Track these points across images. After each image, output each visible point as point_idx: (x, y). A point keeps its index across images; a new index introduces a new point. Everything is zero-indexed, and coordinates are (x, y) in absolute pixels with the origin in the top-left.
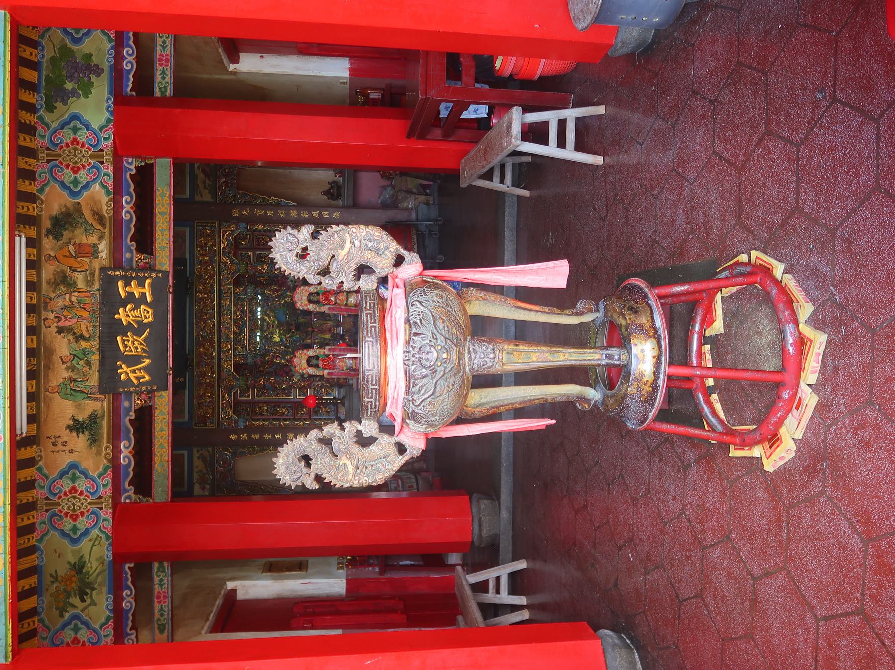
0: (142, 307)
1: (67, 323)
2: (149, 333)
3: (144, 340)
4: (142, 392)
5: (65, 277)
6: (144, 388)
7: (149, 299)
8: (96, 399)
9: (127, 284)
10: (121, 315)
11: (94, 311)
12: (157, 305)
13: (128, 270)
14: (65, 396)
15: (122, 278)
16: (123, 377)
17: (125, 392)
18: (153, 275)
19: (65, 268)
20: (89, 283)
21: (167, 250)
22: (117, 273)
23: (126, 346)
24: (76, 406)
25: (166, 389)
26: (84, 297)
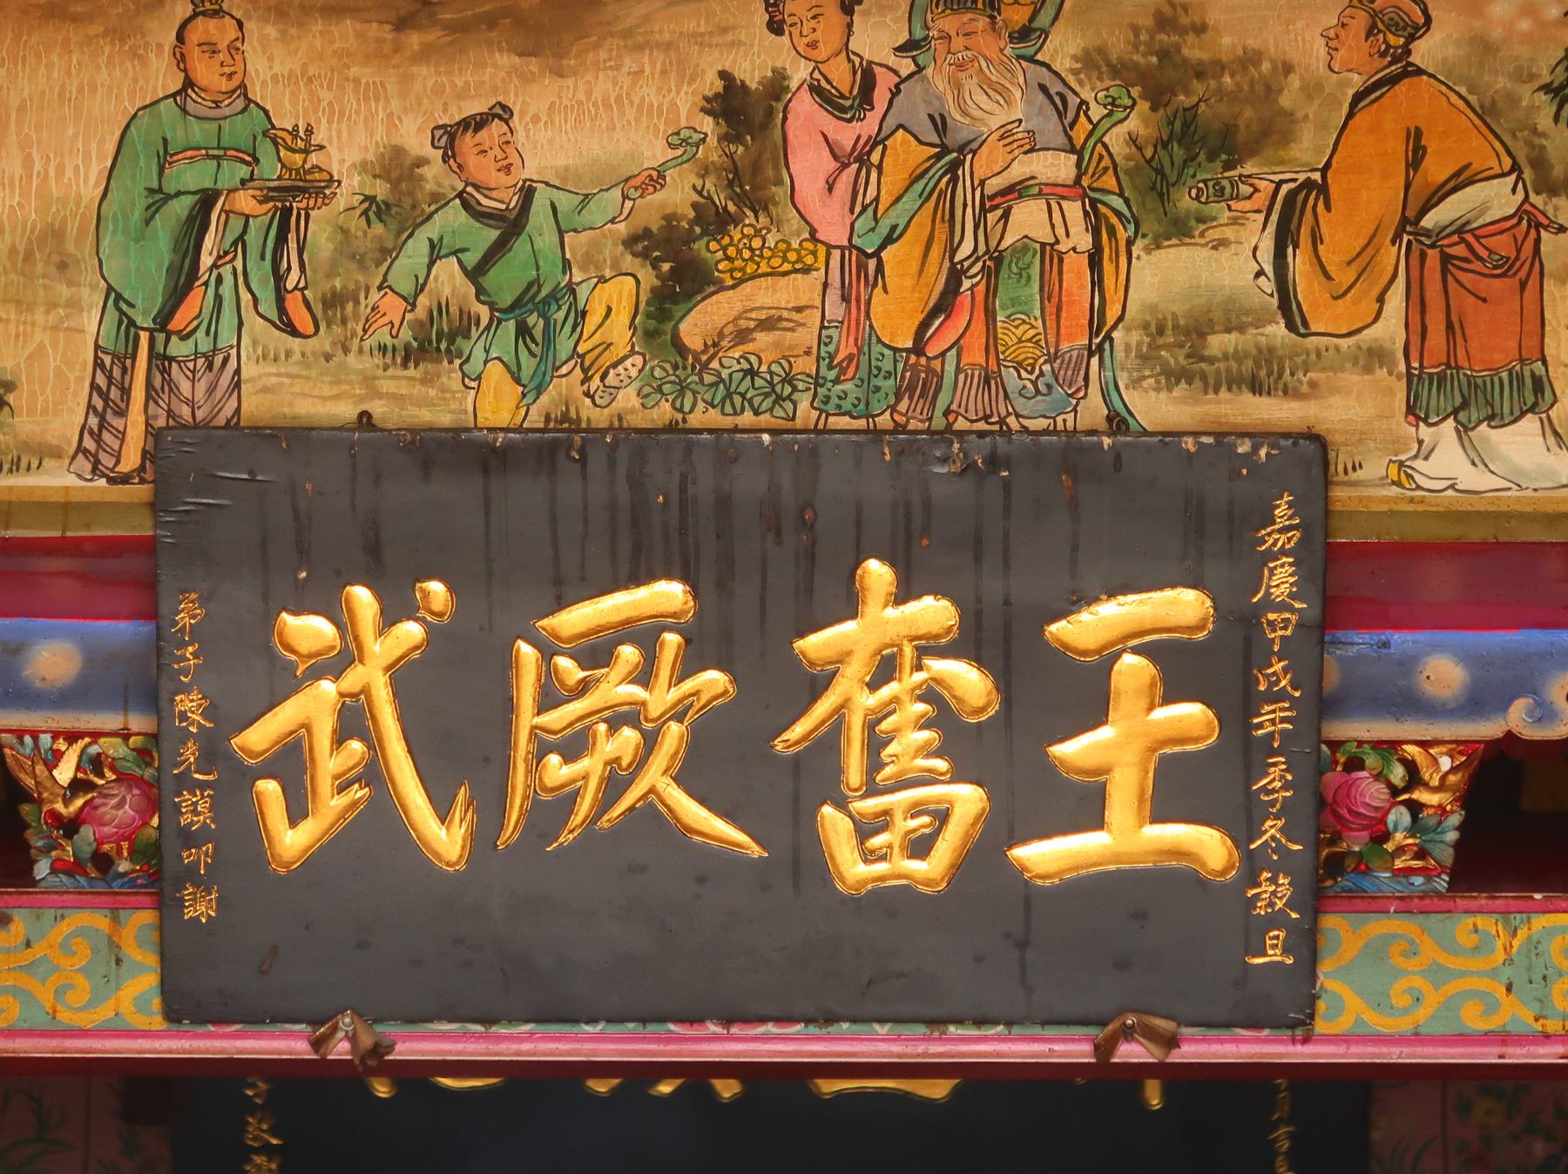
0: (968, 799)
1: (809, 166)
2: (721, 858)
3: (651, 815)
4: (154, 799)
5: (1228, 146)
6: (196, 810)
7: (1045, 856)
8: (107, 400)
9: (1179, 664)
10: (889, 614)
11: (923, 386)
12: (993, 927)
13: (1310, 676)
14: (143, 149)
15: (1239, 622)
16: (308, 630)
17: (160, 649)
18: (1274, 892)
19: (1308, 149)
20: (1183, 348)
21: (1517, 1014)
22: (1281, 580)
23: (595, 652)
24: (56, 234)
25: (180, 1007)
26: (1051, 294)
